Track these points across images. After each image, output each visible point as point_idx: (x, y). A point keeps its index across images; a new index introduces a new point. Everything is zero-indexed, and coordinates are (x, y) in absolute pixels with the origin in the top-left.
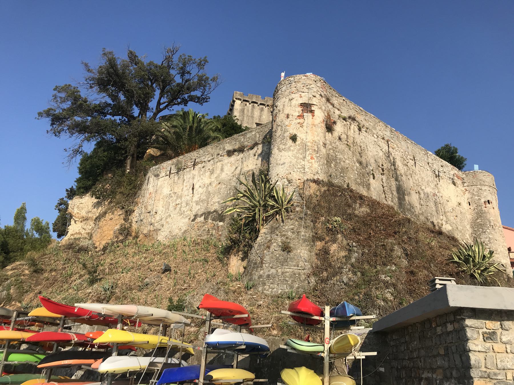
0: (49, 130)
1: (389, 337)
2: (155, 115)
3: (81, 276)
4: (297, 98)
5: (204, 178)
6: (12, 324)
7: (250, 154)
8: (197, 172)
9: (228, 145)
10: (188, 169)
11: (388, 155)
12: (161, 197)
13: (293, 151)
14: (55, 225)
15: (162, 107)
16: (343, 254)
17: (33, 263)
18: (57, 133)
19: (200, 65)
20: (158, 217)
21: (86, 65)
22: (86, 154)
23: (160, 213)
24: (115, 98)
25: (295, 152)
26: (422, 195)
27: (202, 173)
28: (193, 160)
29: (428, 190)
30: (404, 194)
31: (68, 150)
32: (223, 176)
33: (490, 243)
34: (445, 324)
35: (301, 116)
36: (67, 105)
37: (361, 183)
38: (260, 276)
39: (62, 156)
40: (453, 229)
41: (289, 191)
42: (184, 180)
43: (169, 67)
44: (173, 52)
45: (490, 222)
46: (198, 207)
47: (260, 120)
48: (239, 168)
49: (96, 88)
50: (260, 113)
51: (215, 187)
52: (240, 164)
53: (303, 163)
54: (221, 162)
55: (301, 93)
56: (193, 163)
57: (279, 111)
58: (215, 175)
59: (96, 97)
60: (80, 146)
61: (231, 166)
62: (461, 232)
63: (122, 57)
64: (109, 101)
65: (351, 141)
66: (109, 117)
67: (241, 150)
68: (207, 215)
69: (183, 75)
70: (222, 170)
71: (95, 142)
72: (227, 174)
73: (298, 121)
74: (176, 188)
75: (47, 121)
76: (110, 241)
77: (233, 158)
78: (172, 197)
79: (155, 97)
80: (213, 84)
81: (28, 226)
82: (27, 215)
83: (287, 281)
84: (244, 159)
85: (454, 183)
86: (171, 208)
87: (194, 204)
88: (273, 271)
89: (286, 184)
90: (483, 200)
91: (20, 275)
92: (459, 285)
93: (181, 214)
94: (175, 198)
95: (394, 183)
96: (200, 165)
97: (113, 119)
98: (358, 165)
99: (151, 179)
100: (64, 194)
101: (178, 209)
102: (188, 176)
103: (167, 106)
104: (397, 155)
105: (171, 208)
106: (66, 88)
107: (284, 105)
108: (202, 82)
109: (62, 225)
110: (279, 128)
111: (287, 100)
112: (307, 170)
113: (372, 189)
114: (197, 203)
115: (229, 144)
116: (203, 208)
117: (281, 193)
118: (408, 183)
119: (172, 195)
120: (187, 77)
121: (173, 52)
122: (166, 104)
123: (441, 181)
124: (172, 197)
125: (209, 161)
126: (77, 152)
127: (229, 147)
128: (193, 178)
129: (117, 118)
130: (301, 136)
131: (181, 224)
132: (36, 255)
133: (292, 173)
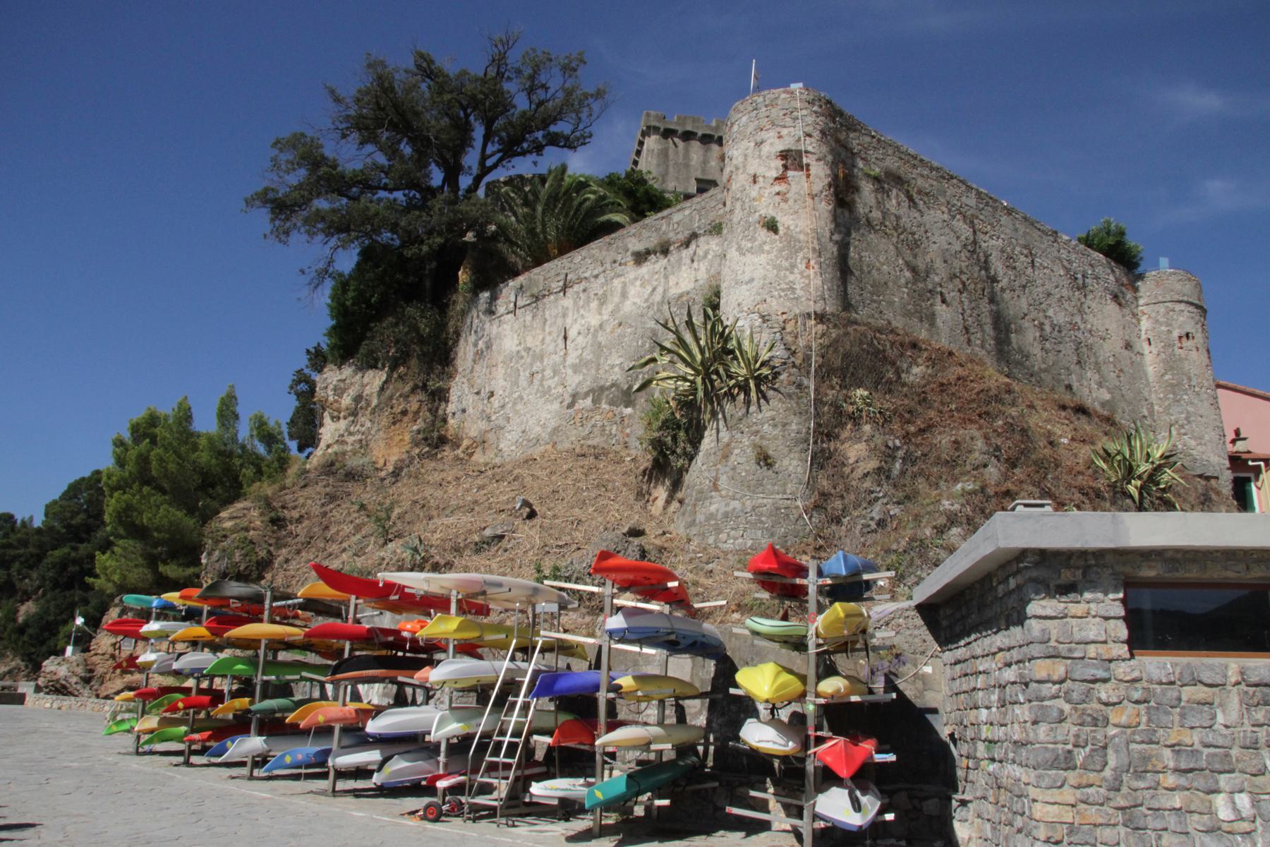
0: (268, 232)
1: (942, 612)
2: (478, 180)
3: (358, 528)
4: (771, 140)
5: (586, 314)
6: (266, 613)
7: (681, 259)
8: (571, 301)
9: (634, 240)
10: (552, 297)
11: (973, 247)
12: (501, 359)
13: (769, 253)
14: (292, 423)
15: (489, 163)
16: (873, 464)
17: (268, 503)
18: (283, 234)
19: (569, 70)
20: (496, 402)
21: (332, 92)
22: (341, 275)
23: (501, 392)
24: (393, 152)
25: (772, 256)
26: (1048, 328)
27: (581, 303)
28: (562, 277)
29: (1061, 318)
30: (1008, 331)
31: (307, 271)
32: (628, 307)
33: (1189, 422)
34: (1006, 580)
35: (781, 179)
36: (299, 175)
37: (916, 311)
38: (711, 516)
39: (298, 286)
40: (1113, 398)
41: (765, 337)
42: (546, 320)
43: (500, 75)
44: (507, 44)
45: (1190, 379)
46: (578, 378)
47: (703, 171)
48: (660, 290)
49: (355, 136)
50: (705, 156)
51: (612, 332)
52: (663, 280)
53: (791, 278)
54: (622, 279)
55: (779, 129)
56: (561, 284)
57: (737, 169)
58: (610, 307)
59: (352, 156)
60: (330, 262)
61: (642, 285)
62: (1130, 403)
63: (401, 64)
64: (382, 159)
66: (382, 194)
68: (597, 393)
69: (530, 91)
70: (624, 295)
71: (358, 250)
72: (635, 304)
73: (777, 188)
74: (529, 339)
75: (262, 216)
76: (405, 456)
77: (645, 269)
78: (522, 357)
79: (475, 144)
80: (596, 106)
81: (244, 431)
82: (239, 409)
83: (762, 522)
84: (669, 268)
86: (523, 381)
87: (570, 371)
88: (736, 504)
89: (757, 324)
90: (1176, 334)
91: (247, 529)
92: (1099, 513)
93: (545, 393)
94: (529, 360)
95: (985, 307)
96: (576, 288)
97: (391, 197)
98: (908, 274)
100: (303, 362)
101: (536, 382)
102: (554, 312)
103: (500, 160)
104: (991, 244)
105: (523, 381)
106: (295, 142)
107: (746, 156)
108: (572, 104)
109: (306, 426)
110: (738, 205)
111: (752, 144)
112: (799, 292)
113: (939, 322)
114: (576, 369)
115: (636, 237)
116: (589, 379)
117: (746, 345)
118: (1017, 305)
119: (523, 353)
120: (541, 94)
121: (507, 44)
122: (499, 155)
123: (1090, 297)
124: (522, 357)
125: (596, 277)
126: (323, 273)
127: (636, 245)
128: (564, 316)
129: (399, 195)
130: (784, 221)
131: (544, 415)
132: (268, 489)
133: (769, 300)
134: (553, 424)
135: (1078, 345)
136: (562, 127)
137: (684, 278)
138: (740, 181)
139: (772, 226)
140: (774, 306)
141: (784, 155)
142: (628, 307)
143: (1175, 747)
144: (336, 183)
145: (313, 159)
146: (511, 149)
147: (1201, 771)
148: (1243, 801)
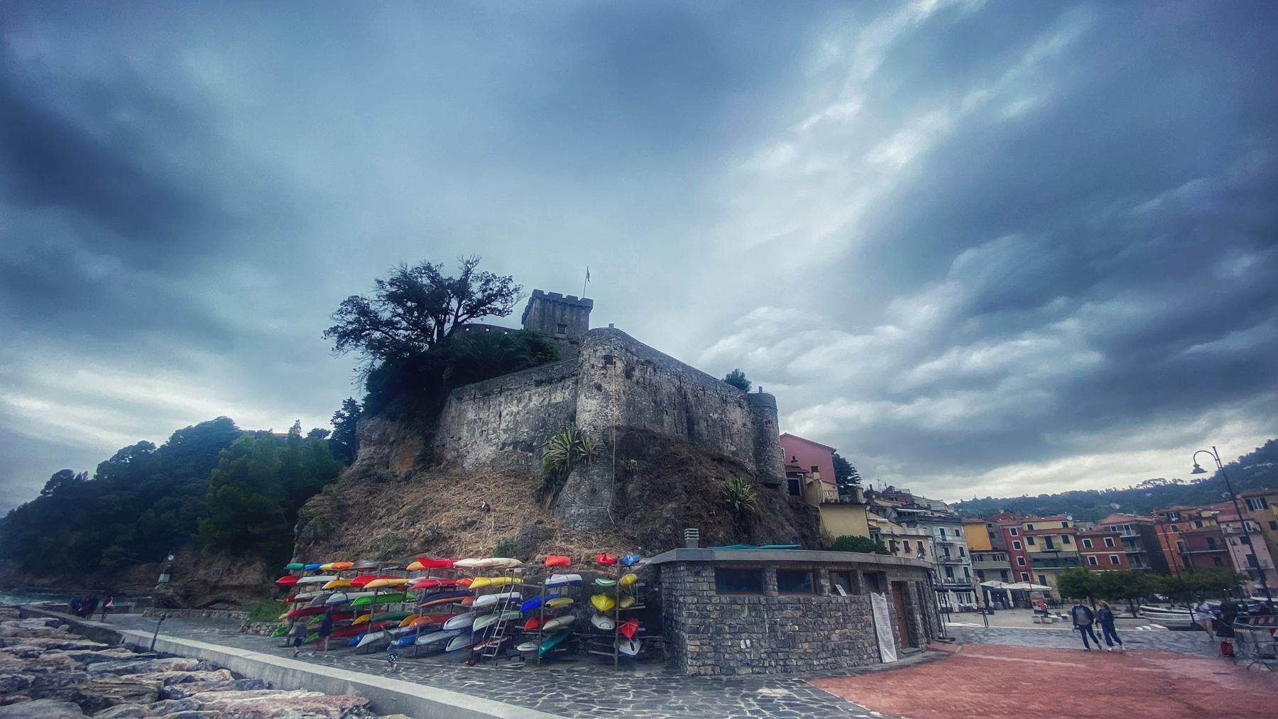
16: (638, 493)
65: (647, 382)
67: (550, 381)
68: (516, 444)
70: (530, 400)
85: (740, 406)
86: (477, 432)
93: (489, 441)
95: (684, 414)
99: (453, 403)
114: (505, 431)
127: (536, 377)
130: (605, 386)
134: (493, 456)
135: (723, 427)
136: (498, 304)
137: (559, 396)
138: (587, 366)
139: (599, 388)
140: (599, 423)
141: (605, 357)
142: (531, 404)
143: (730, 626)
144: (376, 324)
145: (363, 311)
146: (472, 312)
147: (737, 633)
148: (748, 642)
